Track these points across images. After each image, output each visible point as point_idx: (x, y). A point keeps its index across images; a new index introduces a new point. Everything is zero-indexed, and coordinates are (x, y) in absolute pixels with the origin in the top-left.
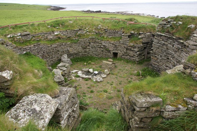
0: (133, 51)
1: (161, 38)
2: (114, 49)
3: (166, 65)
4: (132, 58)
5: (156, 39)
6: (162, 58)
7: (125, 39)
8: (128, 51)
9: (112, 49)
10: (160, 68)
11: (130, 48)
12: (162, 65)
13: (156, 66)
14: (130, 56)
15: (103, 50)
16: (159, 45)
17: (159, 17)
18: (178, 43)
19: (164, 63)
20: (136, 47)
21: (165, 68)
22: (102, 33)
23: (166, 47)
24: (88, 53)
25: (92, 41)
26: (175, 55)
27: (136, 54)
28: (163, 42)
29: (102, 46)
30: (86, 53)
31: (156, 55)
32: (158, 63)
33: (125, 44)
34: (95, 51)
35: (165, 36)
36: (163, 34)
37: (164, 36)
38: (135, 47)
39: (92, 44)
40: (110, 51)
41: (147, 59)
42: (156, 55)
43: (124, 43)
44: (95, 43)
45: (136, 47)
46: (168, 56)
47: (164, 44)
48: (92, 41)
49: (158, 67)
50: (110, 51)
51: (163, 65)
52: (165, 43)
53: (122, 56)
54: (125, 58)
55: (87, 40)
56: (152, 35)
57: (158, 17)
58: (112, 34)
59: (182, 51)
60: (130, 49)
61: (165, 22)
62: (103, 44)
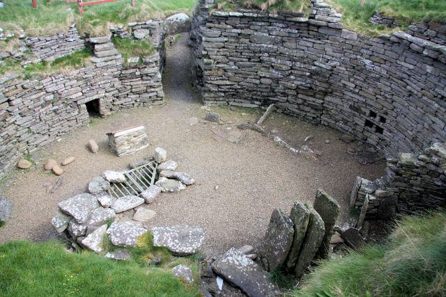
7: (107, 53)
8: (127, 82)
11: (131, 71)
13: (225, 88)
15: (57, 107)
16: (226, 39)
19: (249, 73)
25: (15, 91)
28: (239, 31)
30: (10, 145)
31: (220, 65)
33: (112, 67)
39: (19, 101)
40: (76, 102)
42: (220, 65)
43: (109, 63)
47: (239, 34)
48: (15, 91)
52: (243, 32)
58: (53, 48)
60: (131, 74)
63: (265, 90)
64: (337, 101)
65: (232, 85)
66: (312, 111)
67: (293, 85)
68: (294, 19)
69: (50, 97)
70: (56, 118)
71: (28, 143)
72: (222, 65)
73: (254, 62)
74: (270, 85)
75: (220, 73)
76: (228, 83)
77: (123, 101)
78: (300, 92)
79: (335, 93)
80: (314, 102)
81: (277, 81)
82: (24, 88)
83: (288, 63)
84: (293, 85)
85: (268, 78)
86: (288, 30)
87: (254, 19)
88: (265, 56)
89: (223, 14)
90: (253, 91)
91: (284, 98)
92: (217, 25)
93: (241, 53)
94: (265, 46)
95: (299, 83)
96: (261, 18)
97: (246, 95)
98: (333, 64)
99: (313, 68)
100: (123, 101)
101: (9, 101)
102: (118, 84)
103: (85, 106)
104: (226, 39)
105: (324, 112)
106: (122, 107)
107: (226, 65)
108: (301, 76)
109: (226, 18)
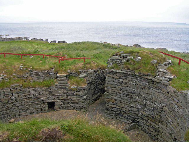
0: (77, 95)
1: (117, 76)
2: (48, 98)
3: (130, 106)
4: (76, 105)
5: (109, 77)
6: (123, 98)
7: (62, 82)
8: (69, 97)
9: (46, 98)
10: (121, 111)
11: (72, 92)
12: (123, 106)
13: (115, 109)
14: (73, 103)
15: (33, 101)
16: (116, 83)
17: (49, 41)
18: (142, 80)
19: (127, 103)
20: (81, 90)
21: (130, 109)
22: (26, 77)
23: (126, 85)
24: (11, 110)
25: (16, 91)
26: (141, 93)
27: (81, 99)
28: (121, 80)
29: (30, 96)
30: (8, 111)
31: (112, 97)
32: (117, 105)
33: (64, 88)
34: (21, 105)
35: (123, 73)
36: (120, 71)
37: (122, 73)
38: (79, 90)
39: (17, 95)
40: (43, 101)
41: (92, 102)
42: (112, 97)
43: (62, 87)
44: (20, 93)
45: (81, 90)
46: (131, 95)
47: (122, 82)
48: (16, 91)
49: (118, 109)
50: (43, 101)
51: (125, 106)
52: (124, 81)
53: (62, 104)
54: (65, 107)
55: (7, 90)
56: (95, 72)
57: (47, 40)
58: (41, 76)
59: (149, 88)
60: (72, 93)
61: (118, 57)
62: (32, 93)
63: (133, 114)
64: (164, 127)
65: (118, 108)
66: (154, 131)
67: (146, 114)
68: (145, 77)
69: (31, 96)
70: (31, 106)
71: (16, 113)
72: (114, 97)
73: (128, 97)
74: (135, 112)
75: (113, 101)
76: (116, 107)
77: (66, 105)
78: (149, 119)
79: (163, 122)
80: (155, 126)
81: (139, 110)
82: (21, 90)
83: (144, 101)
84: (146, 114)
85: (135, 108)
86: (144, 82)
87: (129, 75)
88: (133, 96)
89: (115, 71)
90: (128, 114)
91: (141, 121)
92: (112, 76)
93: (123, 92)
94: (134, 90)
95: (148, 113)
96: (131, 74)
97: (125, 115)
98: (163, 104)
99: (155, 106)
100: (66, 105)
101: (12, 94)
102: (65, 96)
103: (47, 103)
104: (116, 83)
105: (159, 133)
106: (65, 108)
107: (115, 97)
108: (149, 109)
109: (117, 72)
